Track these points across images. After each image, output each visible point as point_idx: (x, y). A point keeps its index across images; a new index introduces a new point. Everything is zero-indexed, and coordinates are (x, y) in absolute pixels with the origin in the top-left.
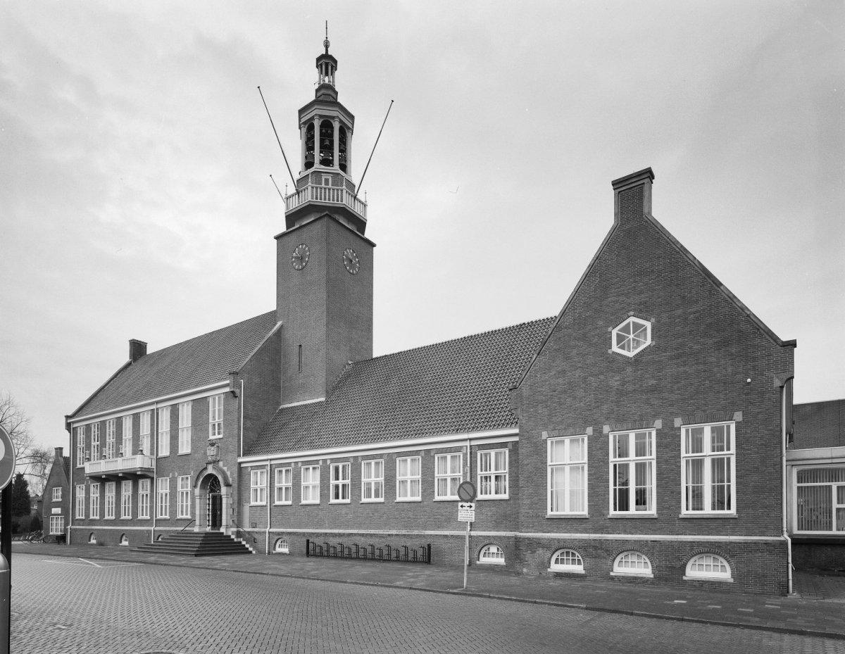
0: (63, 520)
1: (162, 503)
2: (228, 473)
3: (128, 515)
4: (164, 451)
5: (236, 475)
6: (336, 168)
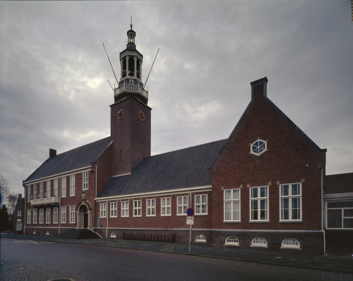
2: (91, 204)
4: (64, 196)
5: (94, 205)
6: (135, 77)
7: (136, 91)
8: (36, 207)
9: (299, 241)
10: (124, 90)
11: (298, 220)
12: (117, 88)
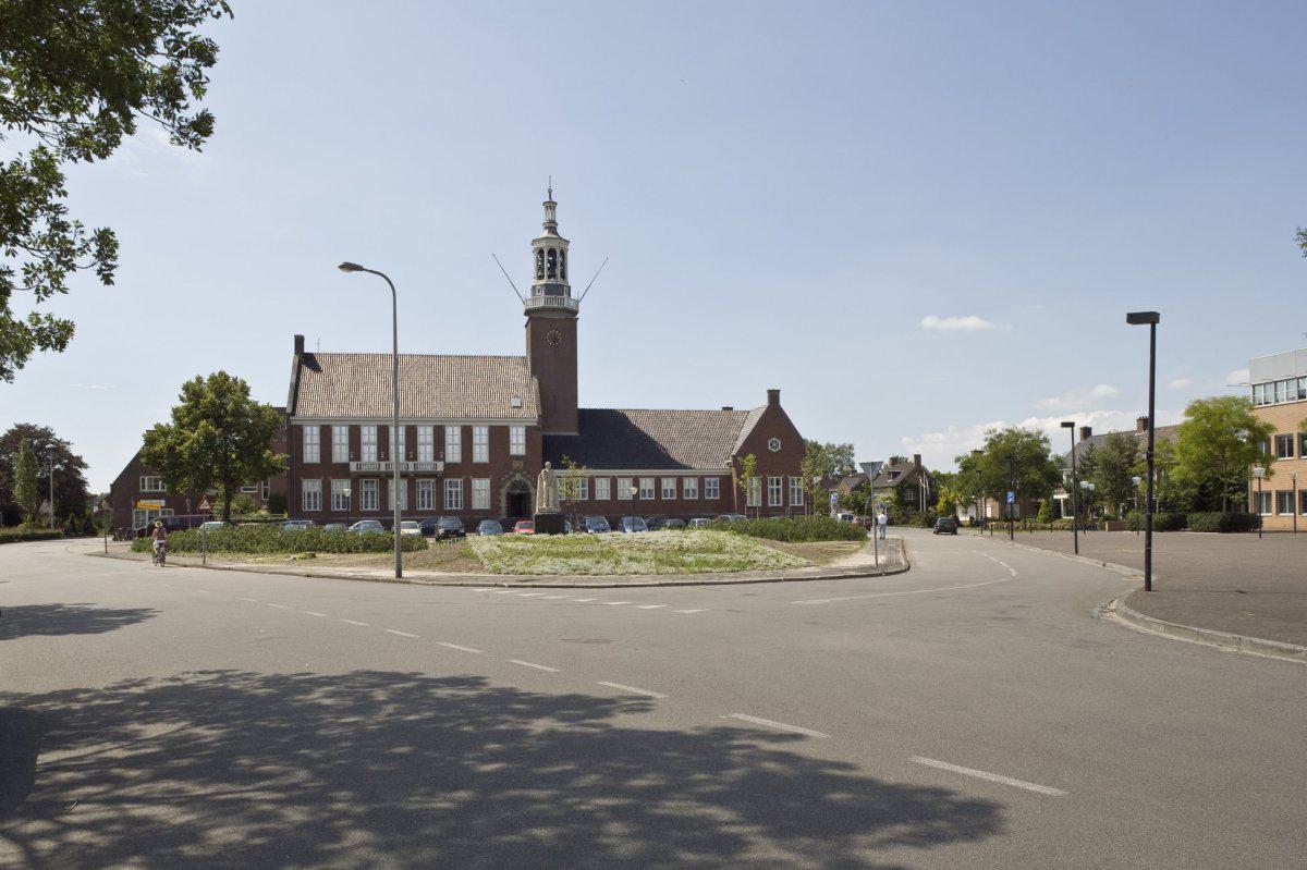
4: (453, 454)
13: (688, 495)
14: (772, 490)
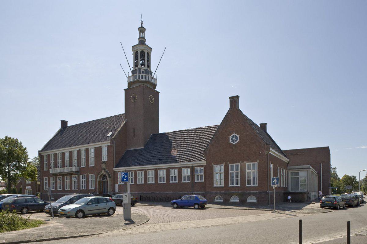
0: (32, 191)
1: (83, 184)
2: (110, 173)
3: (61, 189)
4: (83, 165)
5: (113, 174)
6: (146, 67)
7: (147, 79)
8: (55, 175)
9: (254, 196)
10: (137, 79)
11: (256, 185)
12: (131, 76)
13: (185, 180)
14: (233, 173)
